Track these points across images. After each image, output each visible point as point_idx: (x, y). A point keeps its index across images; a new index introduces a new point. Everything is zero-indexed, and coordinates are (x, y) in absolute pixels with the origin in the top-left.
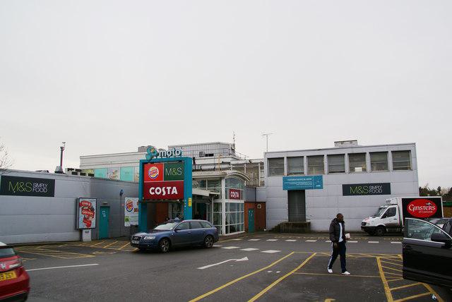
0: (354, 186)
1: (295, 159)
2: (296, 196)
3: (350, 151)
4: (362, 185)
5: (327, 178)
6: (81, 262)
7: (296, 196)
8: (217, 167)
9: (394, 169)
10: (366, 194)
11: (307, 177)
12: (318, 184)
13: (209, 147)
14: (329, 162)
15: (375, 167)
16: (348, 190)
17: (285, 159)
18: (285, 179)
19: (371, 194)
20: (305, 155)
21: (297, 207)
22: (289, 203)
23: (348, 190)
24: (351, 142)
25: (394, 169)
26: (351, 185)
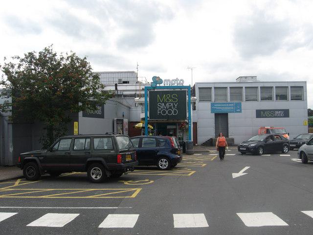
0: (264, 111)
1: (220, 89)
2: (221, 118)
3: (262, 85)
4: (270, 110)
5: (244, 104)
6: (157, 173)
7: (221, 118)
8: (138, 93)
9: (292, 99)
10: (273, 117)
11: (229, 104)
12: (238, 108)
13: (125, 75)
14: (276, 90)
15: (279, 98)
16: (260, 114)
17: (213, 89)
18: (212, 105)
19: (276, 117)
20: (289, 86)
21: (220, 126)
22: (215, 124)
23: (260, 114)
24: (252, 77)
25: (292, 99)
26: (262, 110)
